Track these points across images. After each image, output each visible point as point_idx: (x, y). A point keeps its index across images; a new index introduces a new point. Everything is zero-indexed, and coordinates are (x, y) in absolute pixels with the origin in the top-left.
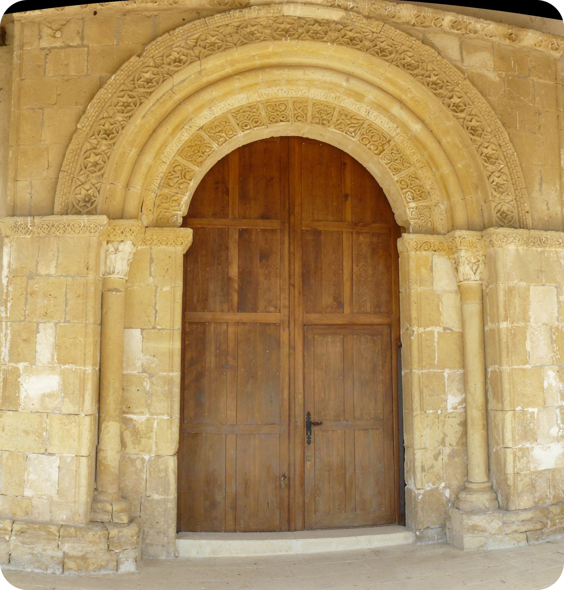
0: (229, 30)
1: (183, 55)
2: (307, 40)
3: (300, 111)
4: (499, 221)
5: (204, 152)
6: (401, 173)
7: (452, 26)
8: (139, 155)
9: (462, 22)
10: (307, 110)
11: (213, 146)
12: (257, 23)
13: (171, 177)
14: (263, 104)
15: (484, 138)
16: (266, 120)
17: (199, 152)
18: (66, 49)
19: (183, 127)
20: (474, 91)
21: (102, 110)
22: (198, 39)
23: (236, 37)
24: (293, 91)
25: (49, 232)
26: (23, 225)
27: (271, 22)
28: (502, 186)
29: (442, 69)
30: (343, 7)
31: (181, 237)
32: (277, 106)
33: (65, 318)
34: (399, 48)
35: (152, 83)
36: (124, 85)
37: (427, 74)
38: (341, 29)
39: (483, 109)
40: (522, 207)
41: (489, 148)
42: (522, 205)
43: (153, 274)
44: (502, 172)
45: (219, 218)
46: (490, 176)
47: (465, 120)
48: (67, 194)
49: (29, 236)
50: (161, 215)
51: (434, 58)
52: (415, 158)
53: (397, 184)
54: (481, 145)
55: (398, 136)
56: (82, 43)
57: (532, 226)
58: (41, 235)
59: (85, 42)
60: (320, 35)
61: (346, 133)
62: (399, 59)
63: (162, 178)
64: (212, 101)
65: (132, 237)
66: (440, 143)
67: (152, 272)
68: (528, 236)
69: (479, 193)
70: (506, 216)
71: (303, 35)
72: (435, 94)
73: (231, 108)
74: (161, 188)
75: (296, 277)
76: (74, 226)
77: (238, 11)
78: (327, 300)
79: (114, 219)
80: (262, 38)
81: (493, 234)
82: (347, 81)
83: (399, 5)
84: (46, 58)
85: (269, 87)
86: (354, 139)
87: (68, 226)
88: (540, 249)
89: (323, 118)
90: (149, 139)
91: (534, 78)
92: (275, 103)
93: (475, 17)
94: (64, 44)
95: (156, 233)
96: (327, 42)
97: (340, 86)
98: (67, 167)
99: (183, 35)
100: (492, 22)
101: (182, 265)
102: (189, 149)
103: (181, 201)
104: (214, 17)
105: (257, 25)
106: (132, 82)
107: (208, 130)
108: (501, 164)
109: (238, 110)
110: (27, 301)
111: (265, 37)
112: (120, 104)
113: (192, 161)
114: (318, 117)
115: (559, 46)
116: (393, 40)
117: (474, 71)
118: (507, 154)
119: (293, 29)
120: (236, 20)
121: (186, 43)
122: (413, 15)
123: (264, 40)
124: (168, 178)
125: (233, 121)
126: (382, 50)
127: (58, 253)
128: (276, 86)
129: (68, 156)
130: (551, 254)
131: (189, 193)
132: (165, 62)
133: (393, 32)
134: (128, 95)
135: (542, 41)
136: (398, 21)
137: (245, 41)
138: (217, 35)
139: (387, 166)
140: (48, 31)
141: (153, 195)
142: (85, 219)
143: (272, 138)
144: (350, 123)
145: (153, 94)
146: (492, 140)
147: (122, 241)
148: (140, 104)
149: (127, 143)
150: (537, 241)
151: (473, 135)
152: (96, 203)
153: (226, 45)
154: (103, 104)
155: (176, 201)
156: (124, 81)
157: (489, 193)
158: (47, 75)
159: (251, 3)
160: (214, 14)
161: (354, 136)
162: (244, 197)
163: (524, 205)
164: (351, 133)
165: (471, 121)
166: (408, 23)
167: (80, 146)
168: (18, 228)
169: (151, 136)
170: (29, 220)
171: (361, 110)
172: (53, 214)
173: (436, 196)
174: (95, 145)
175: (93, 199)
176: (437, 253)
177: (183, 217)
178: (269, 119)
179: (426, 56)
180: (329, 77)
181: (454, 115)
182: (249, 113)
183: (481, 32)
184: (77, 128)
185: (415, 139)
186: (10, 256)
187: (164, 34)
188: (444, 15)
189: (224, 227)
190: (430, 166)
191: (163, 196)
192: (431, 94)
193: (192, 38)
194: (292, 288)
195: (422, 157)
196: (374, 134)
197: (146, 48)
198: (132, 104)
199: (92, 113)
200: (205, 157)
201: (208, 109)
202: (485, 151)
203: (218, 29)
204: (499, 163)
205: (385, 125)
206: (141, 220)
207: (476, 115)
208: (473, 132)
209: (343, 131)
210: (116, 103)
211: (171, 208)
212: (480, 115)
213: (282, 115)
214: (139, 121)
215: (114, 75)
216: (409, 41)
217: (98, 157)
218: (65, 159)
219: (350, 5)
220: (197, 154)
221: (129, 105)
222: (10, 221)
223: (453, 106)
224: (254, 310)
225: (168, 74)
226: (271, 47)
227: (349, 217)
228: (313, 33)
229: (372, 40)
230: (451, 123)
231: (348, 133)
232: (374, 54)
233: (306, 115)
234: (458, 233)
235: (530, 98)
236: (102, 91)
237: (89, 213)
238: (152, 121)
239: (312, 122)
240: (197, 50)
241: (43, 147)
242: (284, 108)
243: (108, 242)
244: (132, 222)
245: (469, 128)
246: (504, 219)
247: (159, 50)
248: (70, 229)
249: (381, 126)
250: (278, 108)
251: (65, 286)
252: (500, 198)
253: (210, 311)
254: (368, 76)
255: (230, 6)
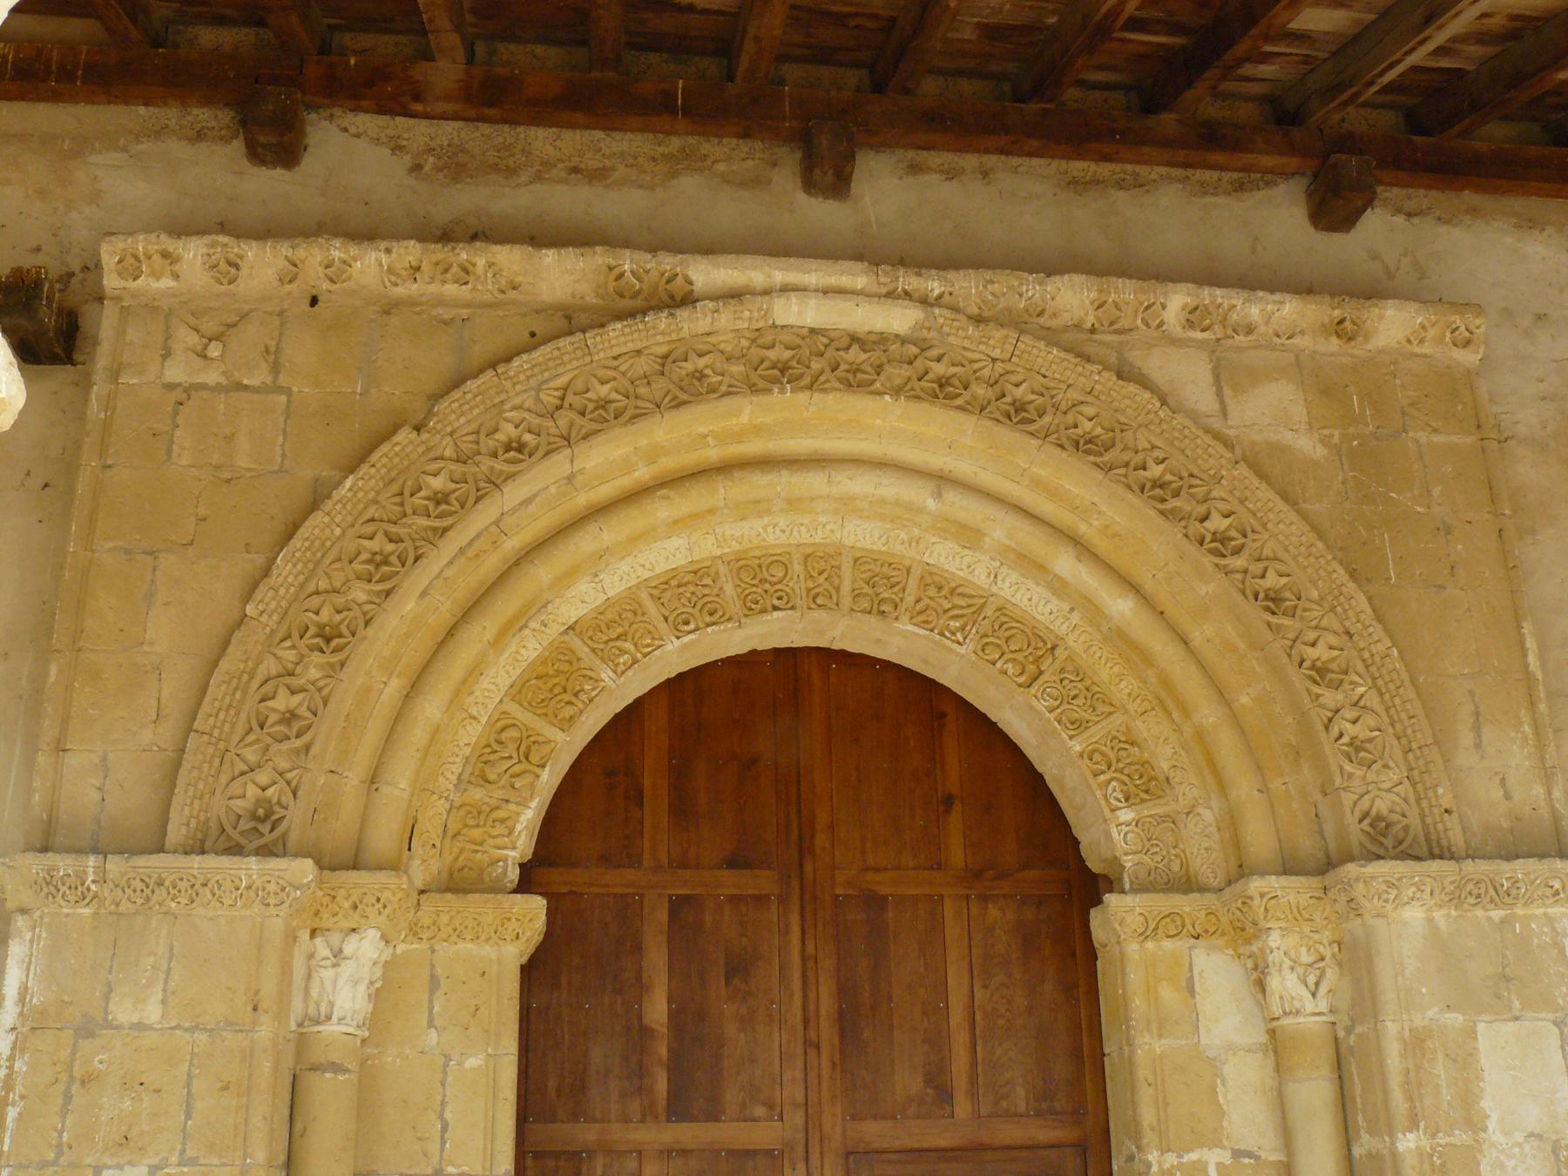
0: (644, 365)
1: (530, 432)
2: (834, 389)
3: (821, 579)
4: (1369, 846)
5: (578, 692)
6: (1093, 730)
7: (1188, 320)
8: (407, 696)
9: (1211, 309)
10: (839, 576)
11: (603, 676)
12: (712, 348)
13: (492, 757)
14: (729, 563)
15: (1302, 618)
16: (735, 607)
17: (565, 691)
18: (231, 394)
19: (525, 626)
20: (1265, 493)
21: (314, 569)
22: (566, 389)
23: (660, 385)
24: (803, 528)
25: (148, 899)
26: (73, 879)
27: (745, 343)
28: (1367, 746)
29: (1176, 442)
30: (916, 295)
31: (514, 920)
32: (764, 569)
33: (183, 1151)
34: (1061, 396)
35: (448, 503)
36: (376, 506)
37: (1138, 459)
38: (916, 357)
39: (1293, 539)
40: (1429, 799)
41: (1321, 645)
42: (1431, 793)
43: (437, 1023)
44: (1364, 707)
45: (618, 867)
46: (1330, 720)
47: (1249, 576)
48: (206, 798)
49: (87, 911)
50: (461, 859)
51: (1151, 416)
52: (1123, 689)
53: (1080, 762)
54: (1297, 637)
55: (1077, 632)
56: (276, 378)
57: (1467, 849)
58: (122, 909)
59: (283, 380)
60: (865, 376)
61: (942, 635)
62: (1062, 427)
63: (467, 758)
64: (602, 556)
65: (382, 918)
66: (1186, 643)
67: (436, 1016)
68: (1458, 878)
69: (1306, 770)
70: (1387, 826)
71: (822, 378)
72: (1162, 513)
73: (648, 574)
74: (462, 786)
75: (824, 1022)
76: (220, 887)
77: (665, 314)
78: (907, 1081)
79: (333, 869)
80: (724, 388)
81: (1357, 880)
82: (938, 495)
83: (1052, 278)
84: (176, 413)
85: (743, 519)
86: (962, 650)
87: (204, 885)
88: (1497, 914)
89: (881, 596)
90: (436, 652)
91: (1421, 433)
92: (757, 562)
93: (1243, 287)
94: (227, 378)
95: (446, 909)
96: (884, 393)
97: (921, 510)
98: (212, 720)
99: (531, 376)
100: (1288, 297)
101: (516, 994)
102: (540, 683)
103: (518, 821)
104: (606, 329)
105: (710, 352)
106: (397, 499)
107: (590, 633)
108: (1357, 684)
109: (662, 580)
110: (69, 1103)
111: (730, 386)
112: (364, 556)
113: (546, 715)
114: (867, 595)
115: (1471, 333)
116: (1045, 377)
117: (1257, 438)
118: (1372, 655)
119: (798, 363)
120: (659, 338)
121: (538, 399)
122: (1088, 302)
123: (730, 393)
124: (483, 759)
125: (652, 609)
126: (1020, 407)
127: (170, 960)
128: (760, 515)
129: (216, 689)
130: (1534, 926)
131: (537, 800)
132: (483, 451)
133: (1043, 354)
134: (386, 534)
135: (1424, 327)
136: (1055, 323)
137: (684, 397)
138: (614, 379)
139: (1052, 716)
140: (188, 339)
141: (442, 805)
142: (251, 868)
143: (753, 652)
144: (949, 606)
145: (451, 533)
146: (1324, 623)
147: (354, 930)
148: (416, 560)
149: (376, 664)
150: (1486, 892)
151: (1273, 613)
152: (285, 824)
153: (636, 407)
154: (319, 555)
155: (502, 821)
156: (378, 493)
157: (1333, 769)
158: (175, 460)
159: (696, 295)
160: (608, 322)
161: (961, 639)
162: (682, 810)
163: (1436, 793)
164: (954, 634)
165: (1263, 576)
166: (1078, 326)
167: (250, 664)
168: (56, 887)
169: (441, 645)
170: (91, 864)
171: (976, 572)
172: (160, 849)
173: (1188, 787)
174: (290, 666)
175: (280, 812)
176: (1201, 942)
177: (521, 865)
178: (744, 603)
179: (1129, 411)
180: (891, 488)
181: (1217, 565)
182: (692, 588)
183: (1262, 329)
184: (246, 615)
185: (1119, 638)
186: (28, 969)
187: (482, 371)
188: (1165, 294)
189: (631, 891)
190: (1165, 709)
191: (470, 808)
192: (1152, 513)
193: (552, 385)
194: (812, 1053)
195: (1141, 685)
196: (1012, 632)
197: (436, 409)
198: (394, 559)
199: (287, 577)
200: (581, 705)
201: (589, 578)
202: (1311, 653)
203: (615, 363)
204: (1351, 683)
205: (1040, 607)
206: (406, 872)
207: (1276, 559)
208: (1271, 605)
209: (932, 630)
210: (353, 556)
211: (491, 842)
212: (1285, 557)
213: (776, 591)
214: (410, 606)
215: (351, 477)
216: (1085, 377)
217: (297, 698)
218: (207, 700)
219: (932, 290)
220: (558, 698)
221: (386, 562)
222: (35, 865)
223: (1212, 541)
224: (713, 1115)
225: (490, 481)
226: (746, 412)
227: (957, 854)
228: (848, 371)
229: (992, 382)
230: (1210, 587)
231: (947, 634)
232: (1001, 418)
233: (838, 589)
234: (1256, 885)
235: (1416, 492)
236: (318, 518)
237: (266, 851)
238: (445, 607)
239: (852, 610)
240: (564, 418)
241: (146, 662)
242: (781, 575)
243: (313, 933)
244: (383, 877)
245: (1261, 596)
246: (1384, 836)
247: (469, 417)
248: (210, 896)
249: (1029, 609)
250: (766, 575)
251: (188, 1057)
252: (1364, 777)
253: (594, 1120)
254: (989, 479)
255: (646, 300)
